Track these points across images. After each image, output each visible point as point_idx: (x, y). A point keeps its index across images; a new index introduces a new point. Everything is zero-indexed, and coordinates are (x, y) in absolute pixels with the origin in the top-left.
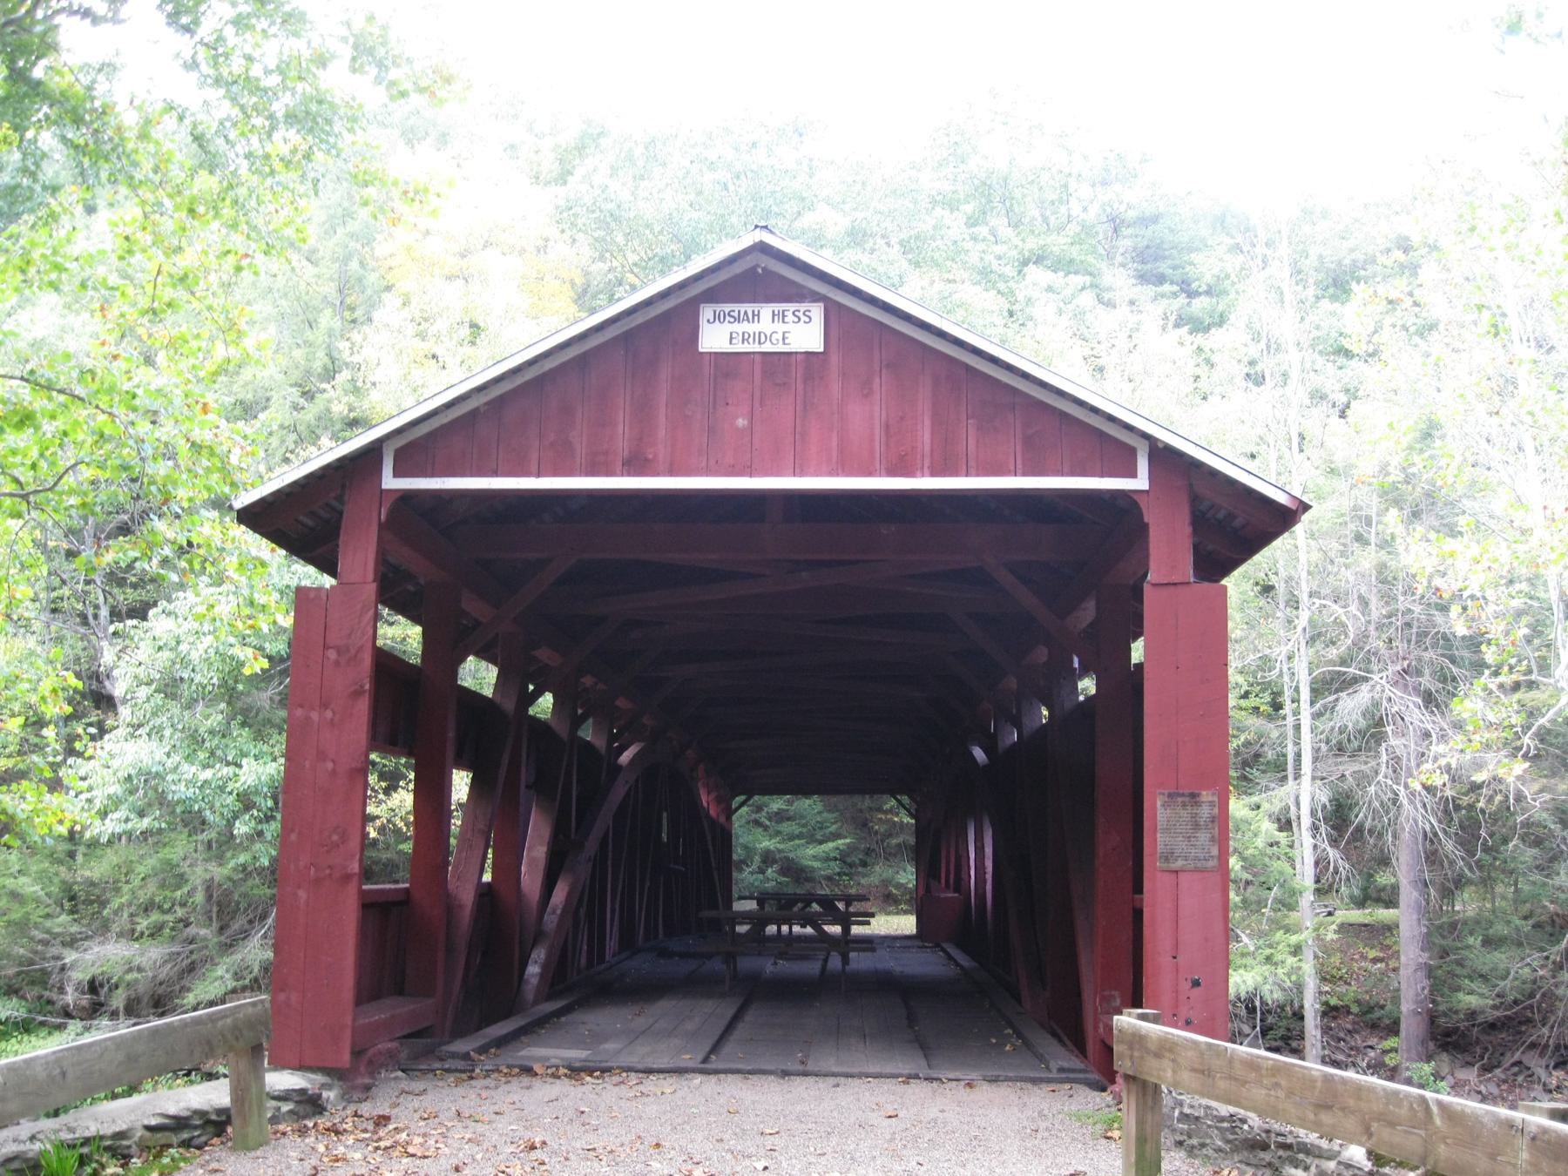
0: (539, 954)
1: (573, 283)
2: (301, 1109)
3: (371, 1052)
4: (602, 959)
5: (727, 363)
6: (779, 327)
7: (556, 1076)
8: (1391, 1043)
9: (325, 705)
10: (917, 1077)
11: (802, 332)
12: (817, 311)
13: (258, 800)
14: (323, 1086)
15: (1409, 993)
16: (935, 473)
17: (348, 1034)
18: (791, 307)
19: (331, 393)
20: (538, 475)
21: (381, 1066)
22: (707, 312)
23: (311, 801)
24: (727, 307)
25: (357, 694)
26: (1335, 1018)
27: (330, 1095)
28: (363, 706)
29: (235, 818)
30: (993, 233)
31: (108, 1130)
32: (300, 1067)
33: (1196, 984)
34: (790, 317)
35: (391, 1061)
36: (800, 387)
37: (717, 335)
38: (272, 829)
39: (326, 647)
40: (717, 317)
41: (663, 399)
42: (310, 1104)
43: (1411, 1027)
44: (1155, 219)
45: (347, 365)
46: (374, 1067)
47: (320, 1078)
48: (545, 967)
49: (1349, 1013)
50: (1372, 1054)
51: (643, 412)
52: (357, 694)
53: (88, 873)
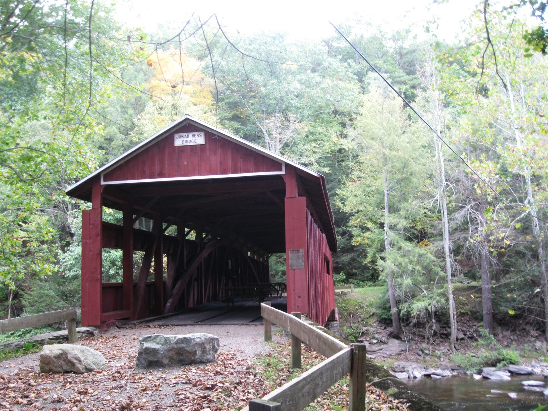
0: (170, 300)
1: (211, 92)
2: (88, 335)
3: (107, 322)
4: (202, 303)
5: (182, 149)
6: (194, 138)
7: (155, 327)
8: (481, 324)
9: (90, 238)
10: (243, 324)
11: (199, 140)
12: (203, 134)
13: (117, 263)
14: (94, 330)
15: (486, 309)
16: (232, 173)
17: (99, 317)
18: (196, 133)
19: (133, 135)
20: (138, 179)
21: (111, 326)
22: (176, 136)
23: (90, 261)
24: (181, 134)
25: (97, 235)
26: (463, 316)
27: (96, 332)
28: (99, 238)
29: (110, 269)
30: (349, 64)
31: (40, 339)
32: (89, 326)
33: (300, 297)
34: (196, 136)
35: (114, 325)
36: (199, 153)
37: (179, 142)
38: (121, 272)
39: (90, 224)
40: (179, 137)
41: (166, 158)
42: (91, 334)
43: (487, 318)
44: (414, 51)
45: (137, 125)
46: (109, 326)
47: (93, 328)
48: (172, 304)
49: (468, 314)
50: (475, 327)
51: (162, 163)
52: (97, 235)
53: (69, 288)
